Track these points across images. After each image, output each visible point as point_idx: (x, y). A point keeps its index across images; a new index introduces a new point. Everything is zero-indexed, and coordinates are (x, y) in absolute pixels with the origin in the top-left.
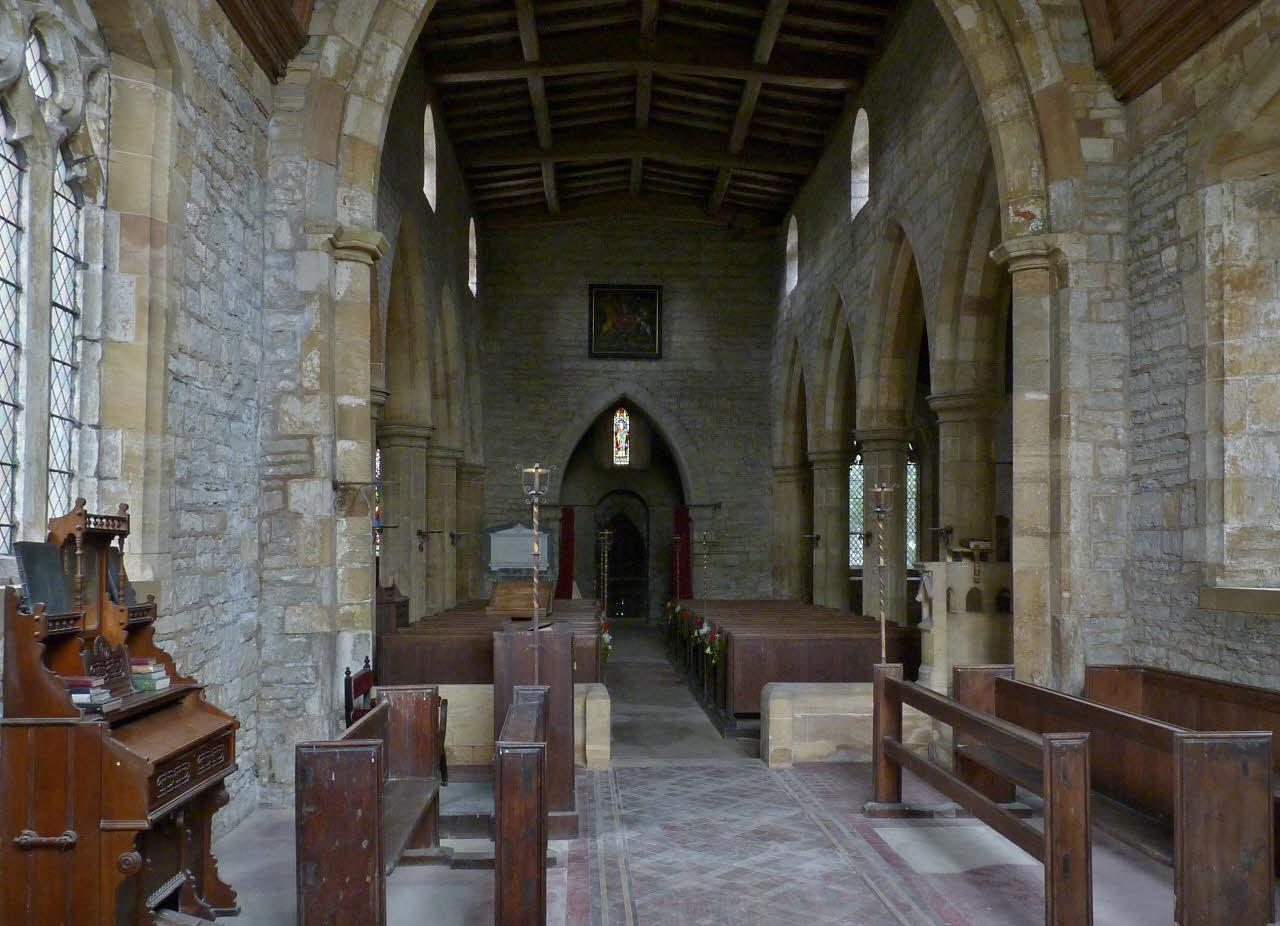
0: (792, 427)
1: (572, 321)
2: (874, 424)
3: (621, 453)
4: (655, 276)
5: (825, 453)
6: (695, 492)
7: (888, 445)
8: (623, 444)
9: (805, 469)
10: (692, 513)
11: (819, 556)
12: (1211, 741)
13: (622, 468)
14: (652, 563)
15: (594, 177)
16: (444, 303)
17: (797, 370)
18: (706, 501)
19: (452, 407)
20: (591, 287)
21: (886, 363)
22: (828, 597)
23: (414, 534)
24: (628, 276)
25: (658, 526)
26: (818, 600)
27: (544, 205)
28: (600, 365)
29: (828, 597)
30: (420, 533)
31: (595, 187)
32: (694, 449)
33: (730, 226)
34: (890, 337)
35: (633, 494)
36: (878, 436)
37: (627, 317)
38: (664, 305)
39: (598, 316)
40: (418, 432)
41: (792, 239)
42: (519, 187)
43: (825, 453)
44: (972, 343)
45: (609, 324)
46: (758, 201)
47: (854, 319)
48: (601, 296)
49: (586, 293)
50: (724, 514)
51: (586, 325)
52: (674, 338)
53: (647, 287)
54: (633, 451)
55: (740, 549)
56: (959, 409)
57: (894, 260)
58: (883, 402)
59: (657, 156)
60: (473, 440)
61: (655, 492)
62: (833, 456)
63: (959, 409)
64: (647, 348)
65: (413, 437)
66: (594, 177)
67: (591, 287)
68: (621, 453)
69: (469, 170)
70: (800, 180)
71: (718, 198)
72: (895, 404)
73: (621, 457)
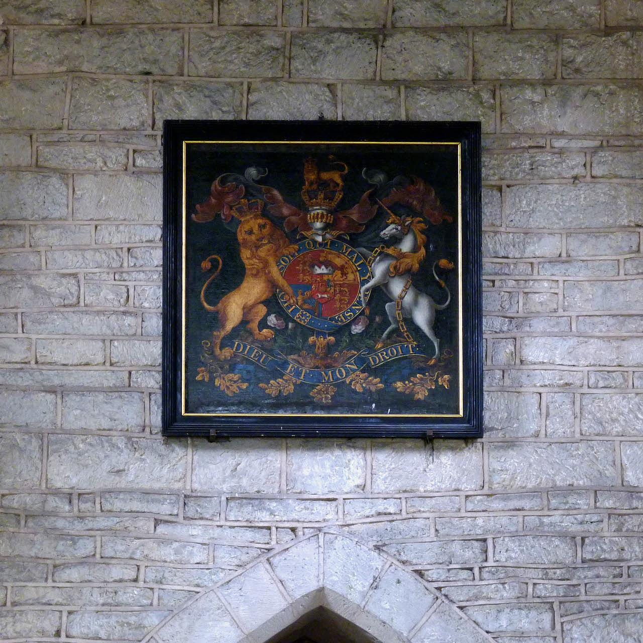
4: (443, 83)
20: (175, 132)
39: (199, 259)
48: (224, 178)
51: (152, 296)
67: (175, 132)
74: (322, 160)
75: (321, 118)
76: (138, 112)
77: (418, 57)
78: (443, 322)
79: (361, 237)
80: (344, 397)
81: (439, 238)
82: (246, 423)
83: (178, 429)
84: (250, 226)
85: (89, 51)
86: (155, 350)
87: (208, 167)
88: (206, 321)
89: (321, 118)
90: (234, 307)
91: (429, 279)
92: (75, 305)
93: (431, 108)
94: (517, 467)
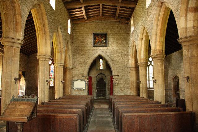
0: (133, 59)
1: (90, 40)
2: (156, 53)
3: (101, 67)
4: (105, 31)
5: (142, 63)
6: (114, 73)
7: (160, 58)
8: (101, 65)
9: (137, 68)
10: (114, 77)
11: (141, 85)
12: (56, 46)
13: (101, 70)
14: (107, 87)
15: (93, 11)
16: (59, 32)
17: (134, 48)
18: (117, 75)
19: (62, 54)
20: (93, 33)
21: (158, 39)
22: (143, 95)
23: (46, 81)
24: (100, 31)
25: (108, 81)
26: (141, 96)
27: (84, 18)
28: (95, 48)
29: (143, 95)
30: (47, 81)
31: (94, 14)
32: (114, 64)
33: (120, 21)
34: (159, 32)
35: (103, 74)
36: (157, 56)
37: (100, 39)
38: (107, 36)
39: (95, 39)
40: (47, 57)
41: (132, 22)
42: (79, 14)
43: (142, 63)
44: (193, 21)
45: (97, 40)
46: (126, 16)
47: (149, 30)
48: (96, 35)
49: (92, 35)
50: (120, 77)
51: (92, 41)
52: (110, 43)
53: (104, 33)
54: (104, 67)
55: (123, 84)
56: (189, 41)
57: (160, 11)
58: (158, 48)
59: (105, 4)
60: (70, 63)
61: (107, 73)
62: (144, 64)
63: (189, 41)
64: (105, 45)
65: (46, 58)
66: (93, 11)
67: (93, 33)
68: (101, 67)
69: (68, 10)
70: (133, 9)
71: (117, 15)
72: (161, 48)
73: (101, 68)
74: (100, 34)
75: (197, 104)
76: (92, 33)
77: (104, 30)
78: (105, 42)
79: (102, 38)
80: (101, 45)
81: (105, 38)
82: (125, 13)
83: (93, 46)
84: (97, 37)
85: (90, 30)
86: (92, 43)
87: (95, 35)
88: (95, 42)
89: (197, 104)
90: (96, 41)
91: (105, 40)
92: (89, 41)
93: (105, 32)
94: (108, 48)
